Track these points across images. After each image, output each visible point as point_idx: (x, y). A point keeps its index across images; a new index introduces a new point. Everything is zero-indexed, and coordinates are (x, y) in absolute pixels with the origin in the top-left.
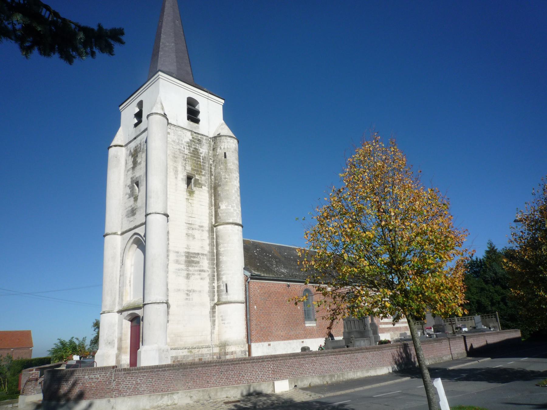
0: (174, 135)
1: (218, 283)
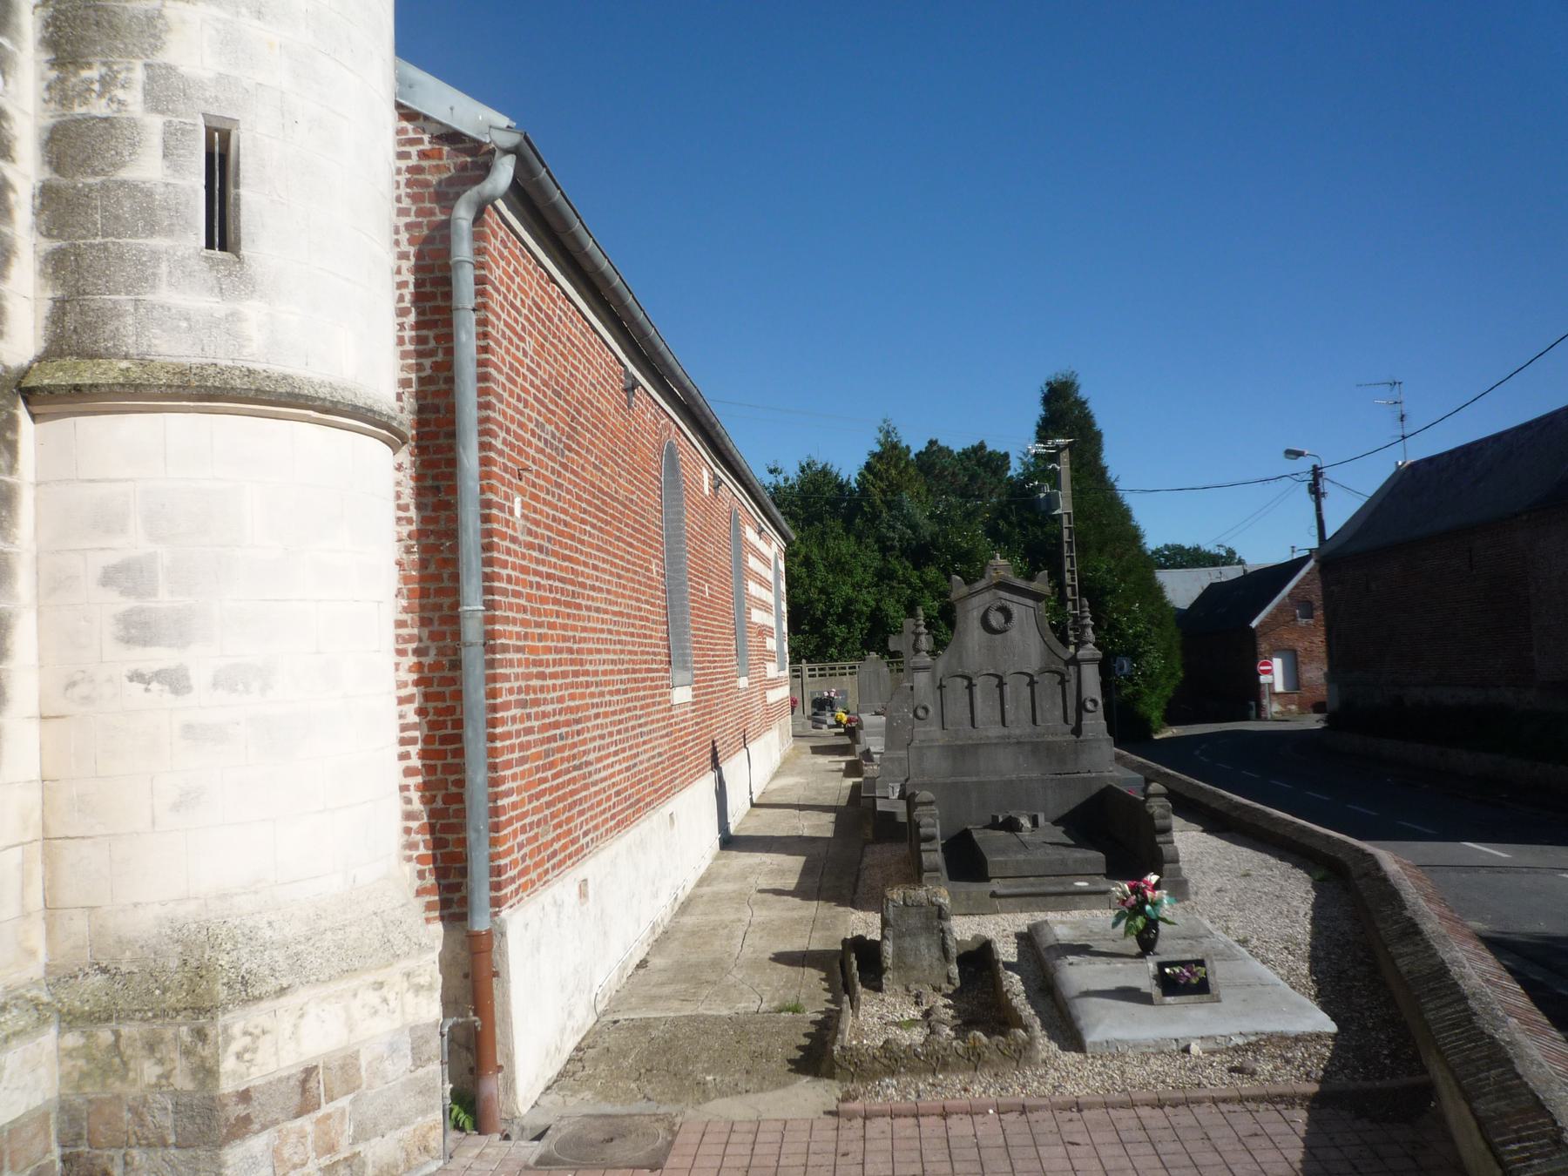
1: (59, 93)
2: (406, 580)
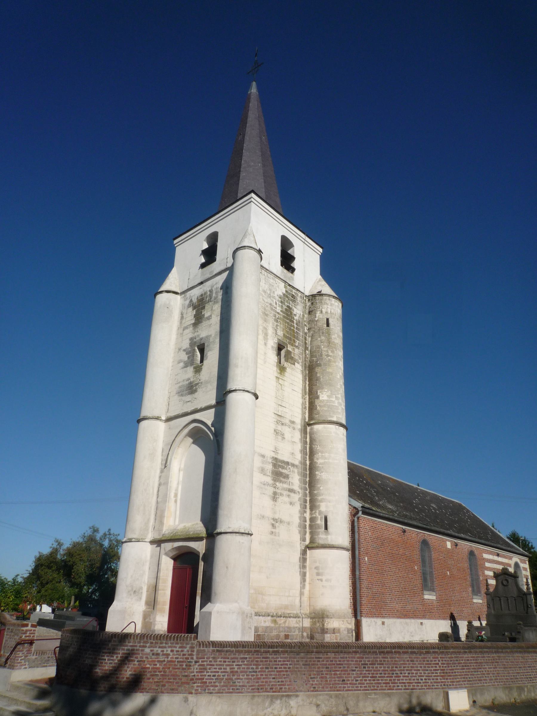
0: (265, 283)
1: (311, 514)
2: (350, 569)
